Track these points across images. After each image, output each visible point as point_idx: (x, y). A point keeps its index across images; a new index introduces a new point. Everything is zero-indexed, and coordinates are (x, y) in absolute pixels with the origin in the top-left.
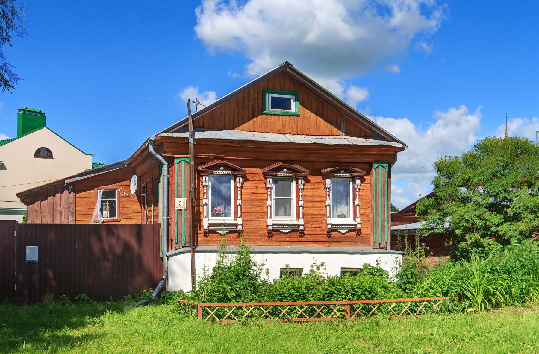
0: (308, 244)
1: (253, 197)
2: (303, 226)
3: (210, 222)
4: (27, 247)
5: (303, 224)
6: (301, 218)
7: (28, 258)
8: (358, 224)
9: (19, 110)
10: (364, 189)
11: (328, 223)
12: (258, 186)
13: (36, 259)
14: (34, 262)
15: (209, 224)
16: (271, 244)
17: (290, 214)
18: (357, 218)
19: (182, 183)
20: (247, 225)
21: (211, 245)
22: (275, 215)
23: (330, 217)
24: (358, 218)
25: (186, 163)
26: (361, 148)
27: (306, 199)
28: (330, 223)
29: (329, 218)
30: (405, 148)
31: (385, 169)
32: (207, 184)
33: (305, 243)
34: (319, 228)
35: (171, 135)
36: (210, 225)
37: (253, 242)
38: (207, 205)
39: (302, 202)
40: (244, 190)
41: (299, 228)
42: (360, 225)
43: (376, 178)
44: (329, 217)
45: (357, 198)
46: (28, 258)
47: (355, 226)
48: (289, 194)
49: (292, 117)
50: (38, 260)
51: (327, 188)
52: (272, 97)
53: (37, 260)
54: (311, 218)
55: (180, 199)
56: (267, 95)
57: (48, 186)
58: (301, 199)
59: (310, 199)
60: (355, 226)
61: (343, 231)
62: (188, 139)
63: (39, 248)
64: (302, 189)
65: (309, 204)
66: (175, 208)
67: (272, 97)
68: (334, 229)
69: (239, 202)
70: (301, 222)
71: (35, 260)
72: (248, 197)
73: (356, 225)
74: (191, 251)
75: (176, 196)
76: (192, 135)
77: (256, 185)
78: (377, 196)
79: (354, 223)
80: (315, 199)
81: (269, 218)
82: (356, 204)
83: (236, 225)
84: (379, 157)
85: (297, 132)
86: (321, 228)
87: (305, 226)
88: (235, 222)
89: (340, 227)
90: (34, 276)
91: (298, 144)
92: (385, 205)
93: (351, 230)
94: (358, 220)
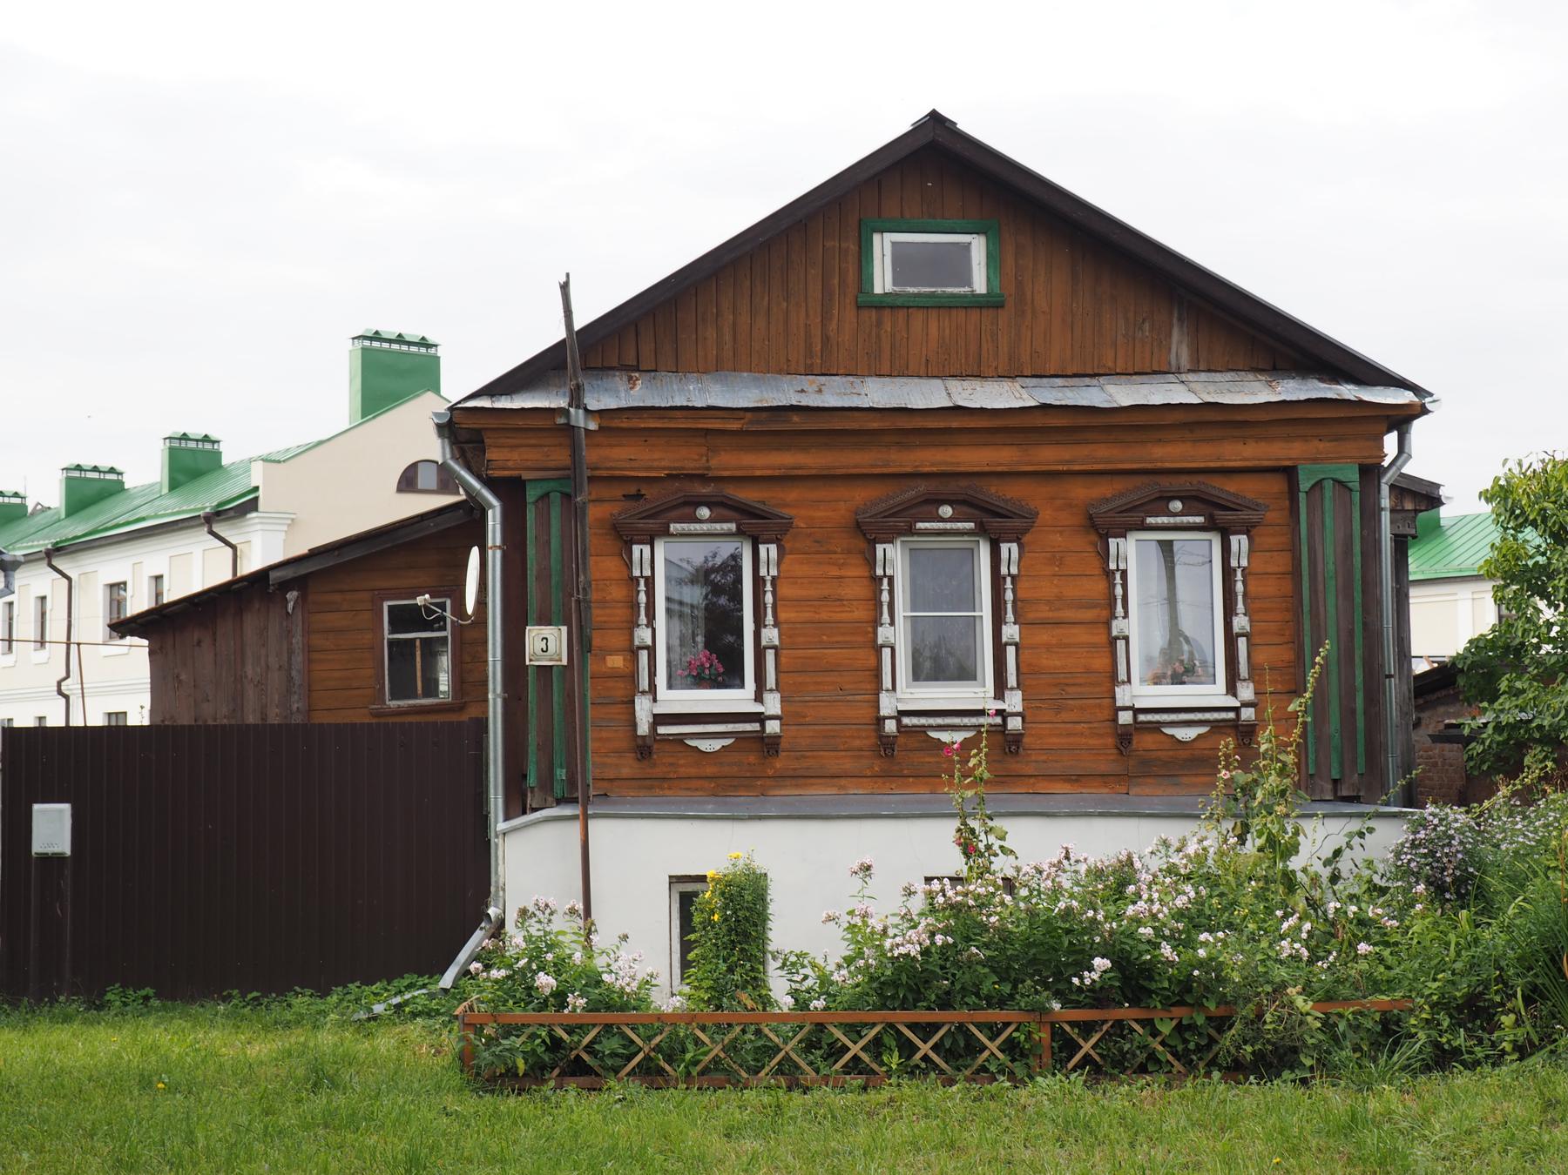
0: (1042, 786)
1: (824, 616)
2: (1019, 719)
3: (660, 709)
4: (36, 807)
5: (1019, 709)
6: (771, 690)
7: (39, 845)
8: (1246, 705)
9: (353, 339)
10: (1269, 570)
11: (1119, 703)
12: (843, 573)
13: (66, 848)
14: (57, 859)
15: (655, 716)
16: (896, 788)
17: (742, 686)
18: (1239, 685)
19: (553, 573)
20: (804, 717)
21: (667, 792)
22: (975, 679)
23: (1129, 681)
24: (1245, 684)
25: (1337, 485)
26: (1082, 421)
27: (1031, 616)
28: (1128, 704)
29: (1126, 687)
30: (1429, 406)
31: (1351, 490)
32: (647, 573)
33: (1032, 780)
34: (1085, 726)
35: (504, 403)
36: (659, 719)
37: (828, 780)
38: (652, 650)
39: (1017, 627)
40: (786, 590)
41: (1238, 715)
42: (1252, 710)
43: (1310, 526)
44: (1123, 682)
45: (1240, 606)
46: (39, 845)
47: (1231, 715)
48: (972, 602)
49: (962, 313)
50: (73, 851)
51: (881, 579)
52: (894, 244)
53: (68, 852)
54: (1056, 685)
55: (548, 631)
56: (876, 238)
57: (212, 594)
58: (1010, 616)
59: (1050, 614)
60: (1231, 715)
61: (1186, 734)
62: (563, 412)
63: (73, 808)
64: (1014, 578)
65: (1044, 636)
66: (527, 663)
67: (894, 244)
68: (1148, 724)
69: (771, 635)
70: (1014, 701)
71: (57, 850)
72: (807, 615)
73: (1236, 710)
74: (581, 817)
75: (532, 614)
76: (576, 398)
77: (835, 572)
78: (1321, 595)
79: (1232, 702)
80: (1069, 614)
81: (887, 690)
82: (1236, 629)
83: (760, 718)
84: (1321, 445)
85: (996, 368)
86: (1095, 725)
87: (1027, 720)
88: (757, 708)
89: (939, 721)
90: (58, 905)
91: (982, 411)
92: (1351, 633)
93: (1217, 727)
94: (1246, 692)
